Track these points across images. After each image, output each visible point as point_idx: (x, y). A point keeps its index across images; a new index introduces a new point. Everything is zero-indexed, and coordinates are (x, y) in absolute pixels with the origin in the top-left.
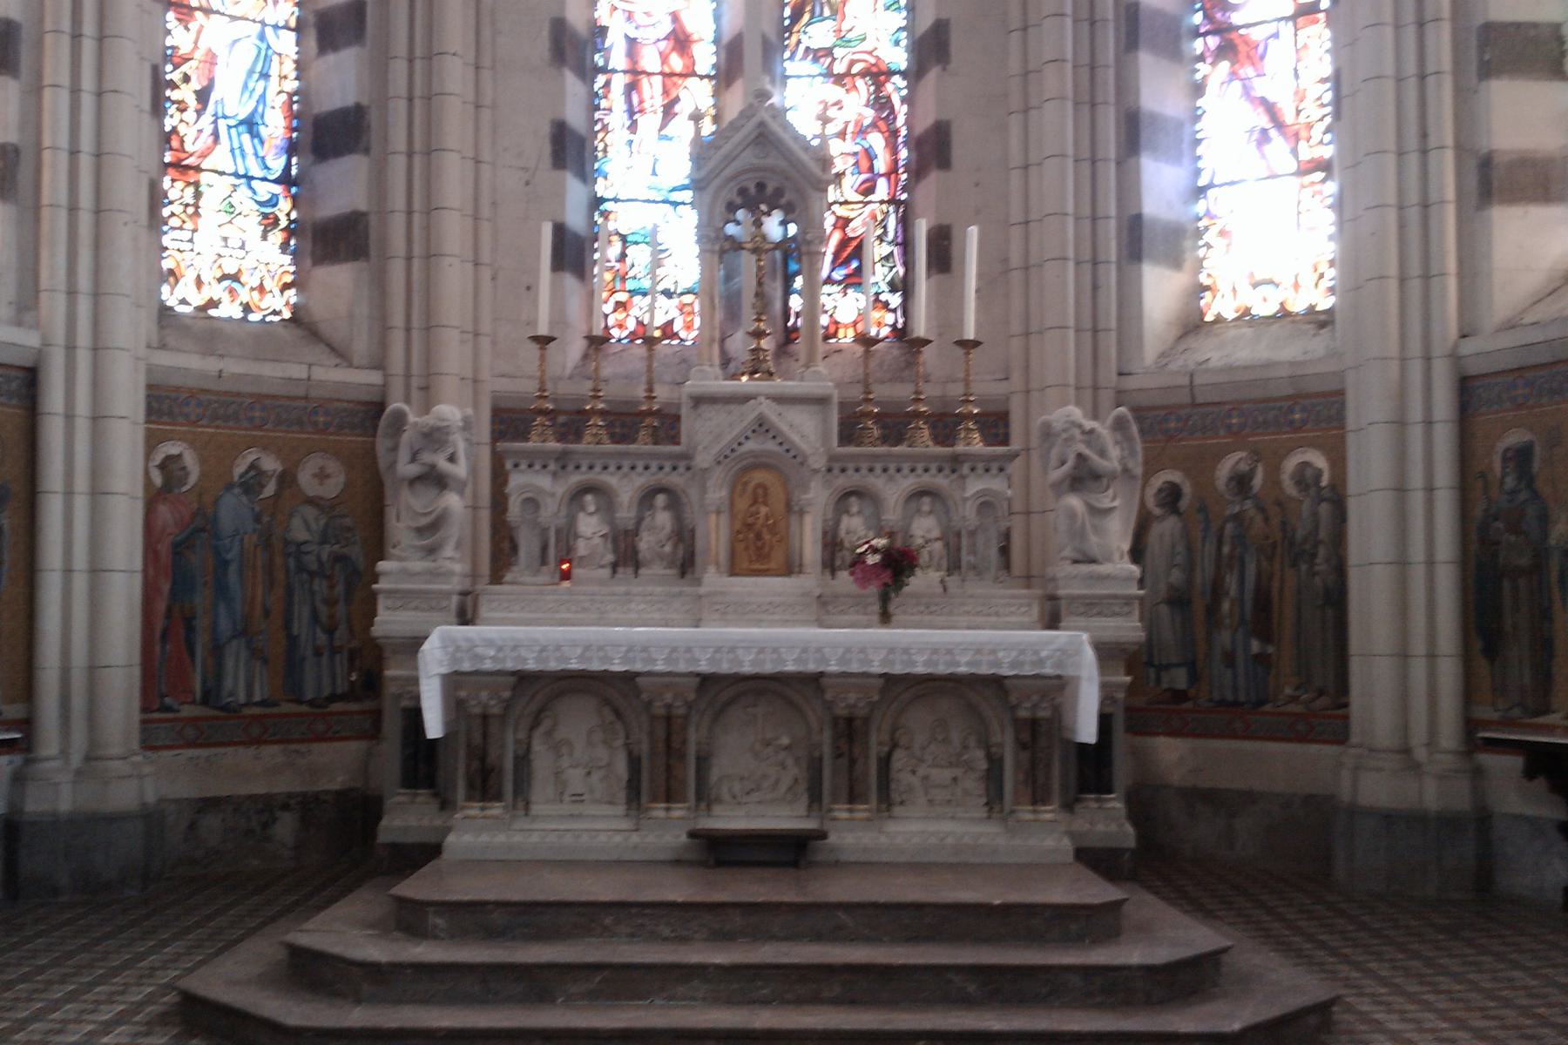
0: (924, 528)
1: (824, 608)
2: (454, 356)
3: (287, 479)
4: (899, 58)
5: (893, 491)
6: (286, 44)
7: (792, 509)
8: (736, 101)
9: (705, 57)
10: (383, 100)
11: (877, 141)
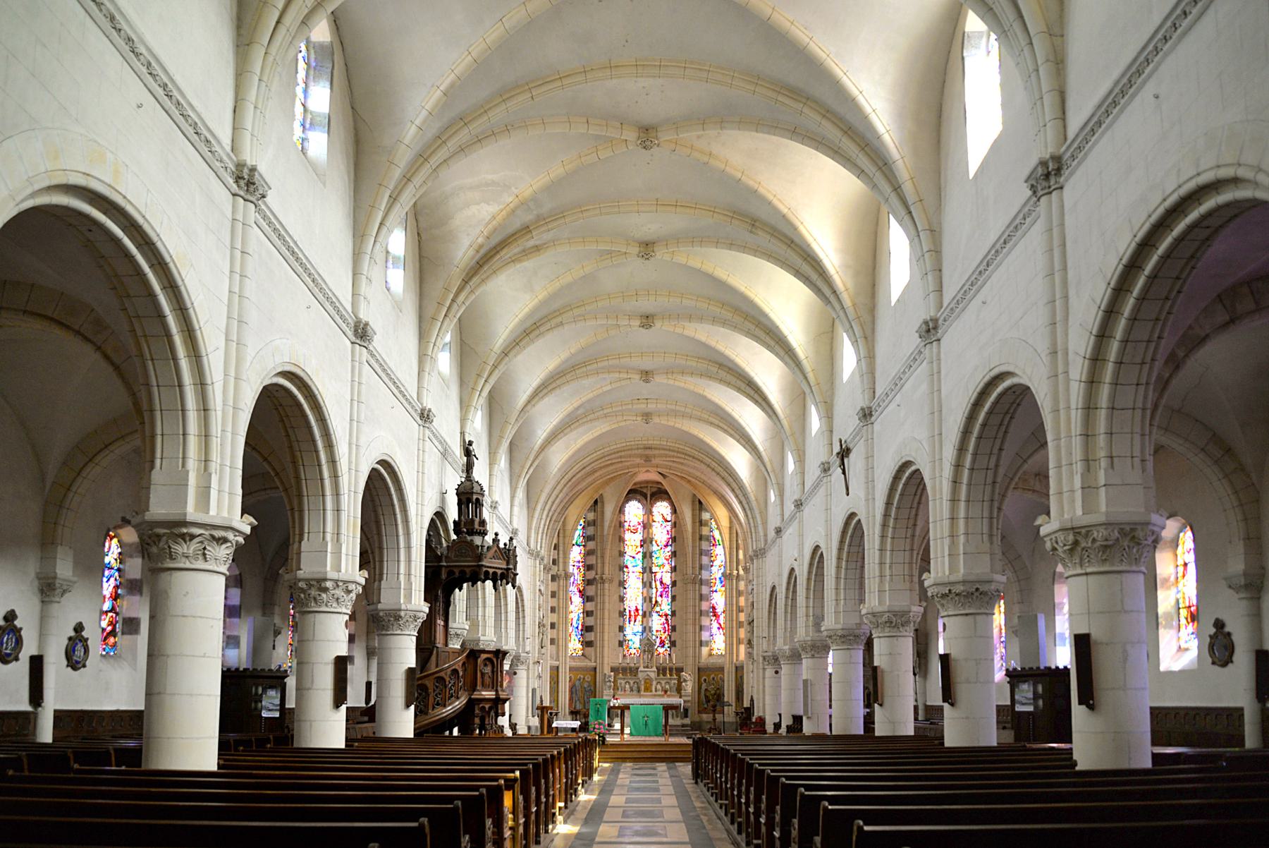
0: (667, 687)
3: (584, 679)
4: (669, 613)
5: (663, 682)
6: (581, 615)
7: (651, 685)
9: (640, 612)
10: (596, 624)
11: (666, 625)
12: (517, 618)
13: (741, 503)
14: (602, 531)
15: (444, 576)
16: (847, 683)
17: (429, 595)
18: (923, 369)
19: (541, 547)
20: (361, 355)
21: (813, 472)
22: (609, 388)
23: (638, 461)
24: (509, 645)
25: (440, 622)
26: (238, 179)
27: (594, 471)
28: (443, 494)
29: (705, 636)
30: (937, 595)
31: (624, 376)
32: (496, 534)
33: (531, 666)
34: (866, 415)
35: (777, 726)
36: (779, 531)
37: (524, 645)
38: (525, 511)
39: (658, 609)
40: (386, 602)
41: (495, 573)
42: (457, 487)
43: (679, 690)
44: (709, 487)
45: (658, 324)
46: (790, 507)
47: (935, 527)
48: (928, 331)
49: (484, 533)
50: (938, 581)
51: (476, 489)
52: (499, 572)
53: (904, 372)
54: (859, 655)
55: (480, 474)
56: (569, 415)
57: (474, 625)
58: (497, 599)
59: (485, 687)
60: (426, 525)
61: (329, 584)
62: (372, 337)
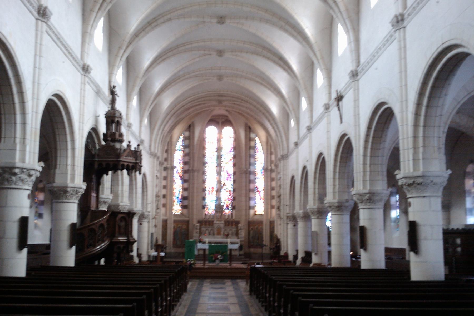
1: (223, 238)
2: (195, 217)
4: (232, 190)
5: (228, 229)
6: (181, 190)
8: (218, 202)
12: (143, 192)
13: (273, 128)
14: (193, 142)
15: (96, 166)
16: (341, 235)
17: (87, 178)
18: (395, 45)
19: (158, 151)
20: (42, 27)
21: (319, 109)
22: (197, 60)
23: (214, 103)
24: (138, 208)
25: (94, 195)
26: (39, 13)
27: (189, 109)
28: (97, 118)
29: (252, 203)
30: (405, 184)
31: (206, 52)
32: (129, 142)
33: (151, 221)
34: (355, 75)
35: (296, 257)
36: (296, 144)
37: (147, 208)
38: (148, 131)
39: (224, 187)
40: (58, 181)
41: (128, 165)
42: (106, 113)
43: (237, 234)
44: (255, 119)
45: (228, 21)
46: (303, 130)
47: (403, 142)
48: (398, 22)
49: (121, 141)
50: (406, 175)
51: (117, 114)
52: (131, 165)
53: (380, 49)
54: (347, 218)
55: (120, 105)
56: (175, 75)
57: (116, 196)
58: (131, 180)
59: (121, 235)
60: (85, 135)
61: (17, 171)
62: (50, 16)
